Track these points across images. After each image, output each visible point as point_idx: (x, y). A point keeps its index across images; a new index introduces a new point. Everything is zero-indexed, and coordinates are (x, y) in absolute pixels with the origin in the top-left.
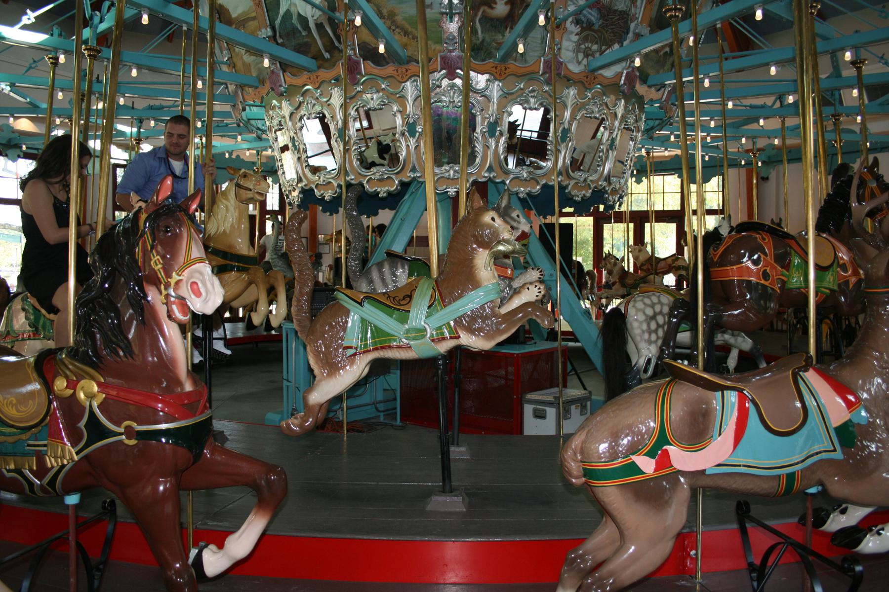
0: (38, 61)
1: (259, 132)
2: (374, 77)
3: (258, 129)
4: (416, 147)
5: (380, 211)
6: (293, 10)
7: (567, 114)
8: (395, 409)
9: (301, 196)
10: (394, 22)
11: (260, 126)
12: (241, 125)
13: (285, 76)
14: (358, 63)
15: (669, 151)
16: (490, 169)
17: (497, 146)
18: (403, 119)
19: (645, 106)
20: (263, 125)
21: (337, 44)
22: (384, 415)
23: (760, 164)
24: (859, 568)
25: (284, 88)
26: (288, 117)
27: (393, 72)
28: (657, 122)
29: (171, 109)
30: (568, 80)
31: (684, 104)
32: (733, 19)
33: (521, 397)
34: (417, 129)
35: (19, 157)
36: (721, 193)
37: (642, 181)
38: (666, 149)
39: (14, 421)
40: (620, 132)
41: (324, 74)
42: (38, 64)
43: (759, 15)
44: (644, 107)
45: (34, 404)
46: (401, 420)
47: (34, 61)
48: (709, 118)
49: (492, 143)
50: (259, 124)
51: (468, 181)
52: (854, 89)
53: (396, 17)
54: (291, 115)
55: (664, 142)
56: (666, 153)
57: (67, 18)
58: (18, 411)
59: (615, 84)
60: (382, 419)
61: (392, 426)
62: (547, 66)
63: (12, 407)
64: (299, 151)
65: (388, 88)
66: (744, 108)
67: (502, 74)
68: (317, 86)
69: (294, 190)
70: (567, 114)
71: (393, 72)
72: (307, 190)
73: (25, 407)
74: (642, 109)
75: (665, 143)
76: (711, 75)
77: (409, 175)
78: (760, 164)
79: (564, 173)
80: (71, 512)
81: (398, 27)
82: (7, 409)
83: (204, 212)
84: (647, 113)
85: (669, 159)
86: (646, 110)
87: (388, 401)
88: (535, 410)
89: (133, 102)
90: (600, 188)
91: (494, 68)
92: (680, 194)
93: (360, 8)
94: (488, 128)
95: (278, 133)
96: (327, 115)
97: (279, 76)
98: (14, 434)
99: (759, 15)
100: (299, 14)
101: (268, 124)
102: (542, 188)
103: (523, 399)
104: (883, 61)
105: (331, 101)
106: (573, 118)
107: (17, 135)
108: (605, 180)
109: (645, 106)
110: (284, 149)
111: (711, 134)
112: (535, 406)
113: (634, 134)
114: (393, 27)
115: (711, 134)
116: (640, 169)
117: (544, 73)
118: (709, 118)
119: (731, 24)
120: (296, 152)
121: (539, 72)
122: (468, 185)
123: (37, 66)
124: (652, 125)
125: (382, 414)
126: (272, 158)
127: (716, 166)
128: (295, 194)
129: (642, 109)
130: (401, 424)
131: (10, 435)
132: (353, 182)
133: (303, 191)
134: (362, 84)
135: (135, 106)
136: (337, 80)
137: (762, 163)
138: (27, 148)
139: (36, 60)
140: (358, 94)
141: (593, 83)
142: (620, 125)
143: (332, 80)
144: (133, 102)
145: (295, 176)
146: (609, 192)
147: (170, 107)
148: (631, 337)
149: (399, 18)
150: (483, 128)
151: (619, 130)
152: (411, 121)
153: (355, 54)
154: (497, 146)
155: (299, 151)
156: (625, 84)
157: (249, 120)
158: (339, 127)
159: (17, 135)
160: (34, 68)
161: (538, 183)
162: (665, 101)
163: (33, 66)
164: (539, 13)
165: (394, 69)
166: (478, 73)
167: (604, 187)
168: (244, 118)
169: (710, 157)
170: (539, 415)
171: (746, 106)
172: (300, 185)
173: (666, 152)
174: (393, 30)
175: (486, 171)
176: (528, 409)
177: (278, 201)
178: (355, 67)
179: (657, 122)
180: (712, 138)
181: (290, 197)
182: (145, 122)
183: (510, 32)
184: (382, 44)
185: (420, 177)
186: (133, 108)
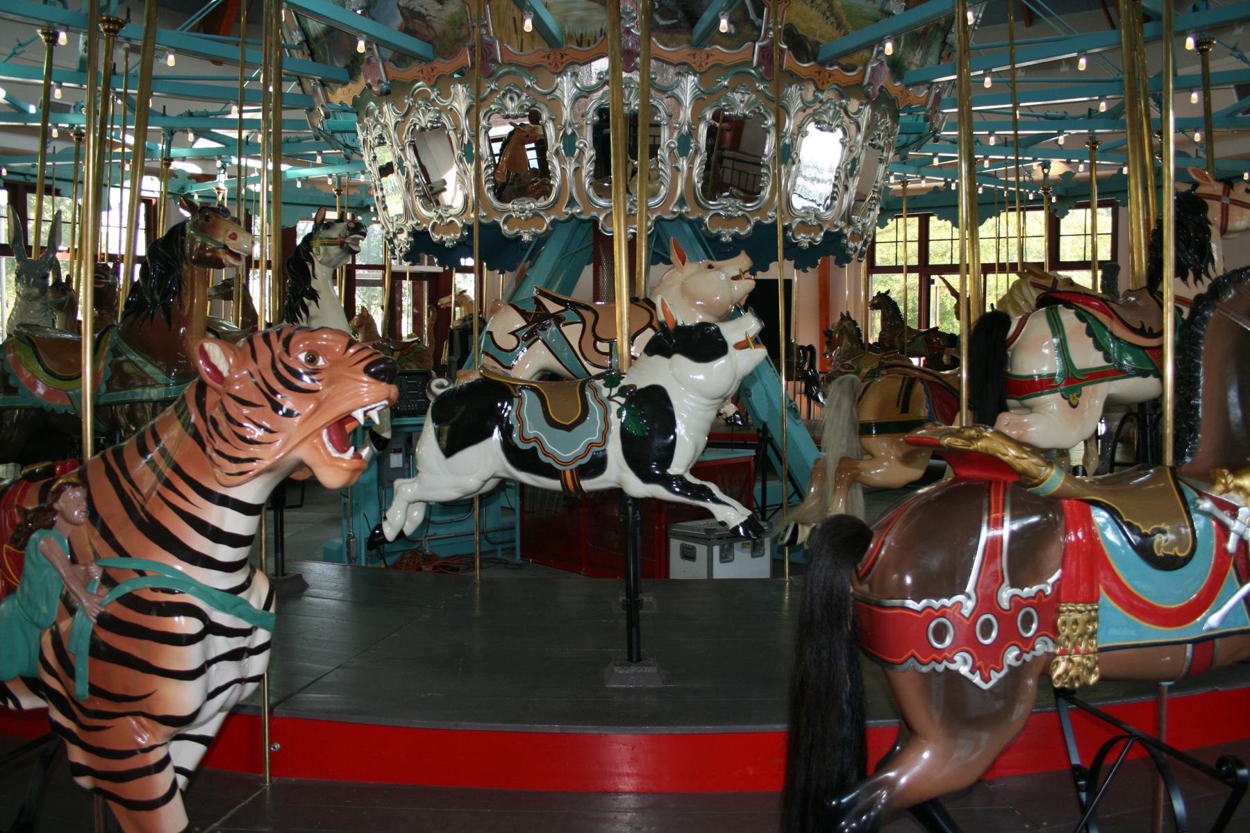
0: (26, 44)
1: (348, 150)
3: (346, 146)
4: (576, 169)
5: (661, 263)
8: (514, 541)
9: (411, 239)
11: (349, 142)
13: (387, 67)
14: (492, 45)
15: (928, 181)
16: (682, 202)
17: (690, 169)
18: (557, 131)
19: (901, 115)
20: (354, 141)
21: (752, 16)
22: (503, 550)
23: (1054, 200)
24: (1243, 772)
25: (385, 84)
27: (541, 59)
28: (913, 137)
29: (219, 116)
30: (791, 75)
31: (146, 130)
33: (667, 528)
34: (577, 144)
36: (1089, 238)
37: (887, 224)
38: (923, 178)
40: (864, 150)
41: (443, 66)
42: (25, 48)
44: (899, 116)
46: (522, 556)
47: (20, 45)
48: (987, 133)
49: (683, 164)
50: (347, 138)
51: (648, 218)
52: (1192, 93)
55: (923, 166)
56: (923, 184)
59: (857, 84)
60: (499, 555)
61: (507, 563)
62: (763, 55)
65: (535, 86)
66: (1035, 119)
67: (559, 64)
69: (401, 231)
71: (541, 59)
74: (895, 118)
75: (923, 169)
76: (994, 70)
77: (564, 210)
78: (1054, 200)
79: (689, 199)
83: (957, 226)
84: (903, 126)
85: (925, 193)
86: (901, 120)
87: (503, 529)
88: (683, 548)
89: (164, 107)
91: (691, 56)
92: (1062, 232)
94: (678, 142)
96: (448, 126)
97: (378, 67)
101: (361, 137)
102: (754, 229)
103: (669, 532)
104: (1236, 54)
108: (842, 219)
109: (901, 115)
110: (386, 170)
111: (990, 157)
112: (682, 542)
113: (885, 154)
115: (990, 157)
116: (885, 208)
117: (759, 64)
118: (987, 133)
121: (752, 61)
122: (649, 224)
123: (23, 51)
124: (904, 141)
125: (499, 547)
126: (367, 188)
127: (993, 203)
128: (403, 237)
129: (895, 118)
130: (521, 562)
133: (415, 234)
135: (167, 113)
136: (460, 72)
137: (1057, 199)
138: (8, 172)
141: (828, 82)
142: (865, 140)
143: (454, 73)
144: (164, 107)
145: (401, 211)
146: (849, 235)
147: (216, 114)
148: (483, 485)
150: (672, 142)
151: (863, 147)
152: (569, 132)
153: (488, 33)
154: (690, 169)
157: (334, 132)
158: (683, 131)
161: (749, 221)
162: (931, 108)
163: (18, 51)
165: (543, 54)
167: (841, 230)
169: (985, 189)
170: (688, 554)
171: (1038, 117)
173: (923, 182)
175: (676, 204)
176: (675, 545)
178: (488, 53)
179: (913, 137)
180: (992, 161)
181: (396, 241)
182: (178, 135)
184: (724, 18)
185: (580, 213)
186: (164, 114)
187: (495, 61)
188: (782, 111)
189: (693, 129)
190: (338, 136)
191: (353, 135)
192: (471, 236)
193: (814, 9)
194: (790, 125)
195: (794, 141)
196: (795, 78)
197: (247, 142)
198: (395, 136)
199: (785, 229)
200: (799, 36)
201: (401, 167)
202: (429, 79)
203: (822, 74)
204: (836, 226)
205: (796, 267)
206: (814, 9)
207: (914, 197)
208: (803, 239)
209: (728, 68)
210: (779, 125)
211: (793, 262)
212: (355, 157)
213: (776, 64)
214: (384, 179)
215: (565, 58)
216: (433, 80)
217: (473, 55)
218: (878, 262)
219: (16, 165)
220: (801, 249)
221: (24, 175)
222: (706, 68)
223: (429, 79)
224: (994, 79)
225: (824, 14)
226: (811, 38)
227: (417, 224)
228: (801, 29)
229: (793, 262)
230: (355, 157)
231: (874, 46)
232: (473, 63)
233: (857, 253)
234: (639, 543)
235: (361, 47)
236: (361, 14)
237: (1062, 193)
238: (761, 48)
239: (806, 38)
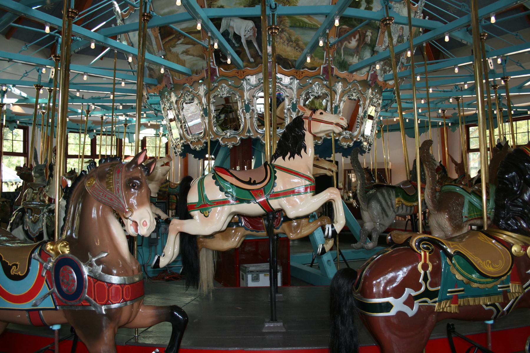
1: (156, 112)
2: (224, 78)
3: (155, 110)
4: (250, 118)
6: (230, 30)
7: (338, 97)
10: (298, 45)
11: (157, 108)
12: (147, 107)
18: (242, 103)
26: (174, 102)
32: (431, 41)
35: (15, 128)
39: (493, 274)
42: (28, 74)
43: (447, 39)
45: (503, 263)
50: (156, 107)
53: (299, 42)
54: (176, 101)
57: (46, 47)
58: (493, 267)
63: (489, 266)
64: (181, 122)
68: (191, 84)
70: (338, 97)
72: (185, 145)
73: (498, 265)
77: (246, 134)
80: (56, 334)
81: (299, 48)
82: (486, 267)
90: (359, 141)
92: (22, 143)
93: (217, 38)
95: (168, 111)
98: (491, 283)
99: (447, 39)
100: (235, 33)
104: (519, 65)
105: (199, 93)
106: (340, 100)
107: (14, 115)
114: (297, 48)
117: (323, 74)
119: (430, 44)
120: (179, 123)
127: (425, 127)
131: (487, 283)
132: (213, 140)
133: (184, 145)
134: (218, 82)
135: (84, 97)
137: (451, 124)
139: (27, 71)
140: (216, 88)
149: (301, 43)
155: (181, 122)
156: (370, 80)
157: (151, 104)
159: (14, 115)
160: (26, 76)
164: (319, 40)
165: (236, 72)
166: (285, 75)
168: (149, 103)
172: (182, 141)
174: (297, 49)
177: (74, 154)
183: (356, 57)
186: (83, 98)
187: (216, 76)
188: (333, 92)
189: (298, 101)
190: (153, 106)
191: (159, 105)
192: (207, 146)
193: (289, 47)
194: (246, 95)
195: (367, 109)
196: (338, 79)
197: (116, 109)
198: (175, 106)
199: (336, 141)
200: (285, 58)
201: (178, 118)
202: (190, 83)
203: (298, 73)
204: (359, 139)
205: (343, 156)
206: (289, 47)
207: (392, 125)
208: (345, 144)
209: (312, 77)
210: (242, 97)
211: (341, 154)
212: (159, 114)
213: (330, 73)
214: (171, 123)
215: (304, 74)
216: (192, 83)
217: (207, 73)
218: (70, 153)
219: (22, 120)
220: (344, 149)
221: (25, 123)
222: (301, 78)
223: (190, 83)
224: (421, 77)
225: (295, 48)
226: (290, 58)
227: (185, 142)
228: (284, 55)
229: (341, 154)
230: (159, 114)
231: (371, 66)
232: (207, 76)
233: (367, 149)
234: (272, 276)
235: (162, 71)
236: (163, 58)
237: (454, 122)
238: (324, 68)
239: (288, 59)
